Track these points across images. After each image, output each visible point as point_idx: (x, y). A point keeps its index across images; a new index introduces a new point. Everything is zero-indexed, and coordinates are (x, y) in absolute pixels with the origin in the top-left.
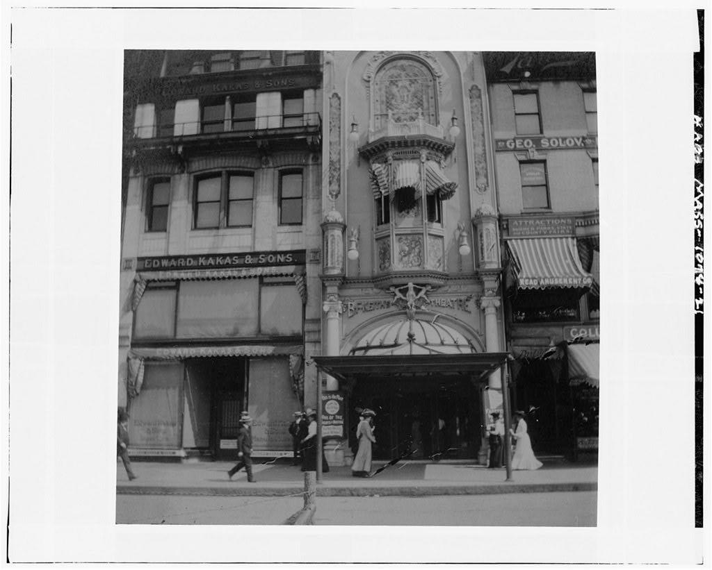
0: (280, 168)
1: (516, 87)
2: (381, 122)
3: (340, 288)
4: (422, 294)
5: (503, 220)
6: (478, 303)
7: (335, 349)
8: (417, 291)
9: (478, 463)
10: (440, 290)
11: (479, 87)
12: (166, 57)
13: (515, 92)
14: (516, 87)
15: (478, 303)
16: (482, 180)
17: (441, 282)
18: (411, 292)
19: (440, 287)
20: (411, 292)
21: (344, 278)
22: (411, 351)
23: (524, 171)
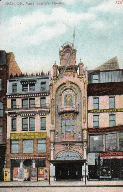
0: (22, 98)
1: (94, 97)
2: (85, 167)
3: (54, 144)
4: (71, 146)
5: (35, 176)
6: (82, 148)
7: (52, 159)
8: (70, 145)
9: (81, 180)
10: (75, 145)
11: (85, 97)
12: (9, 77)
13: (93, 98)
14: (94, 97)
15: (82, 148)
16: (84, 120)
17: (75, 143)
18: (68, 145)
19: (74, 144)
20: (68, 145)
21: (55, 142)
22: (103, 81)
23: (94, 118)
